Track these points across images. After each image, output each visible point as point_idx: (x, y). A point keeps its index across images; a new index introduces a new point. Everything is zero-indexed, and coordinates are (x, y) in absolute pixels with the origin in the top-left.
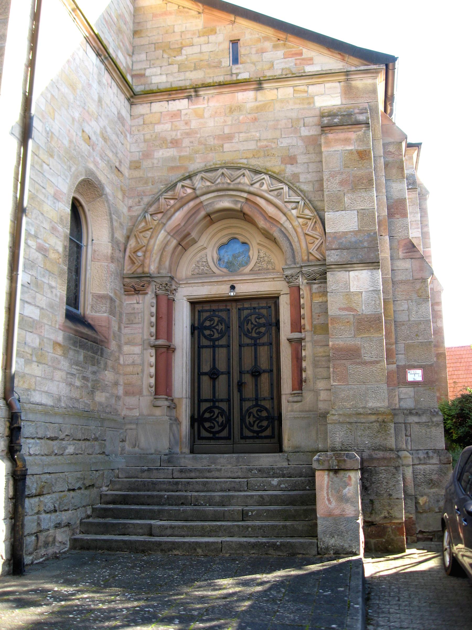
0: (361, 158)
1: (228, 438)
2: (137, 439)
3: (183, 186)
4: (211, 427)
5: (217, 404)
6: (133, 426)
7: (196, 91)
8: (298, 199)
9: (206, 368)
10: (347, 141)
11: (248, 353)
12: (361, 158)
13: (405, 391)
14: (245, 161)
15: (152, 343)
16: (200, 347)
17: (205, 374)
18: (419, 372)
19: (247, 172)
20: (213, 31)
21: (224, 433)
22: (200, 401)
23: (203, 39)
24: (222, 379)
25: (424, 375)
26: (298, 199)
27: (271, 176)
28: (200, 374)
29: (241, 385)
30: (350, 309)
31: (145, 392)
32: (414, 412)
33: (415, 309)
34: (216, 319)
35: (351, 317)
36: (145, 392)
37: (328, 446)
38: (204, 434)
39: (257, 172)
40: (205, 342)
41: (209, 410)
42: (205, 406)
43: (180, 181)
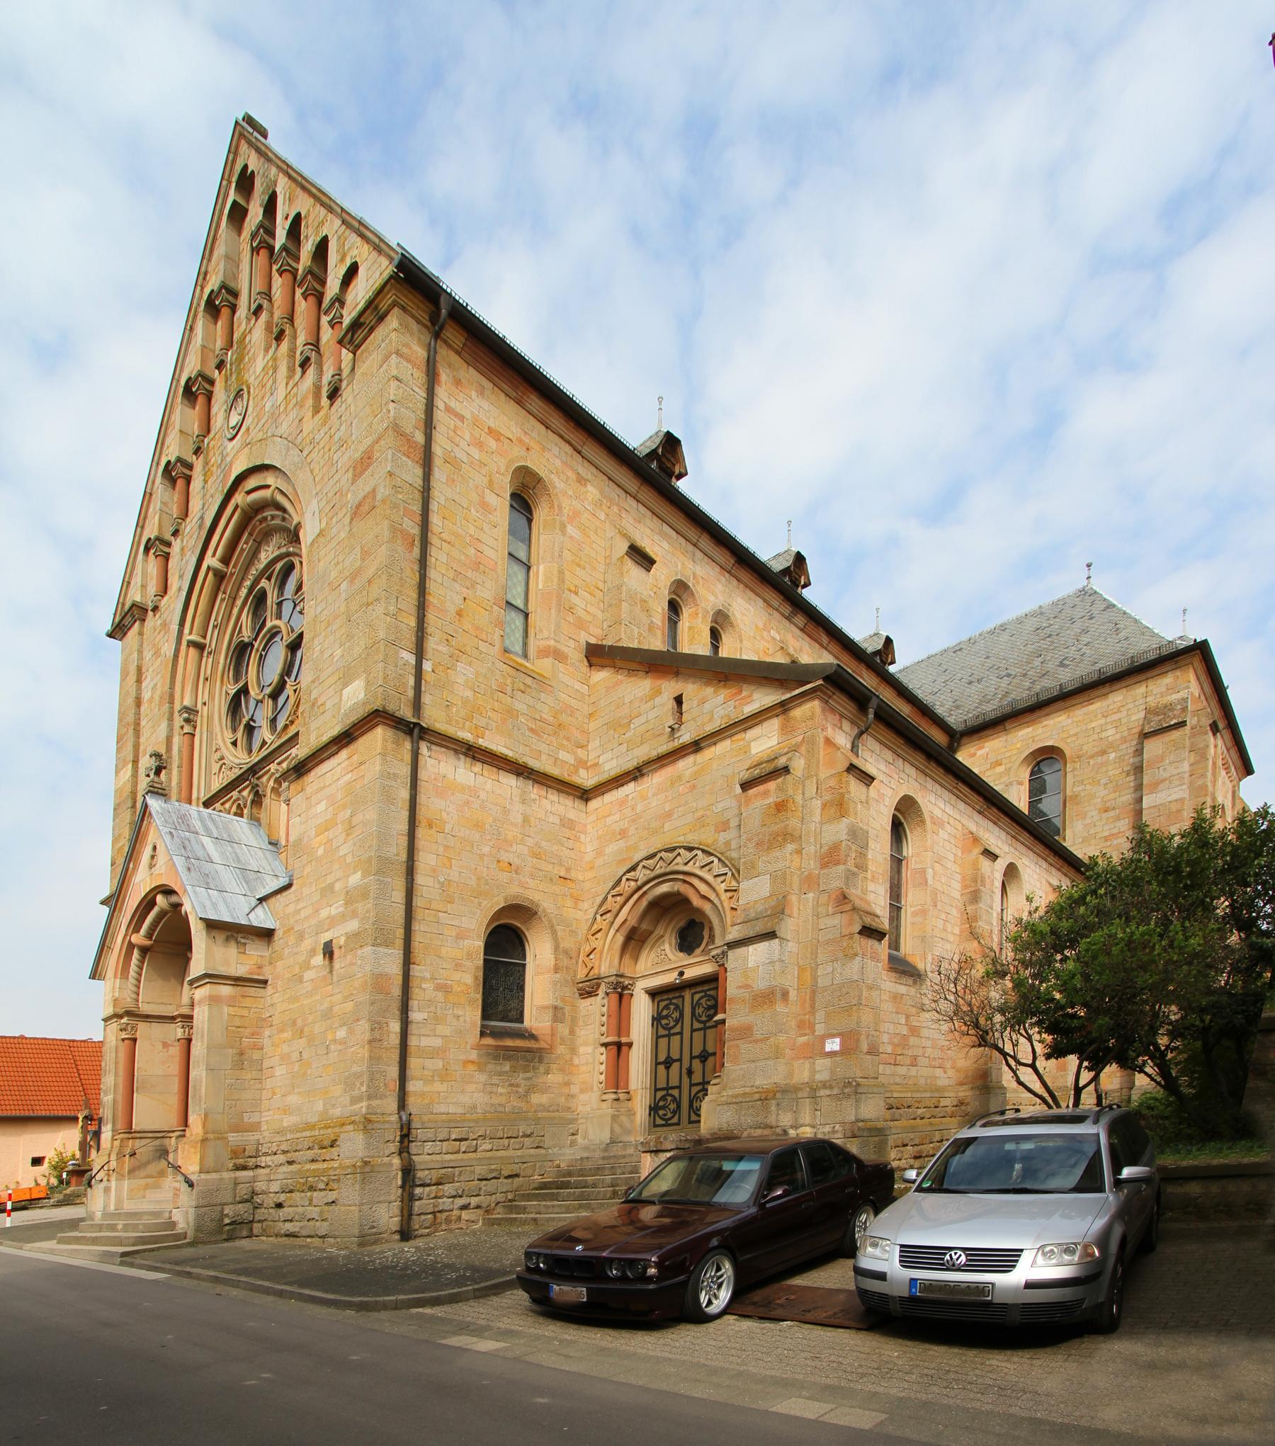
0: (779, 811)
1: (678, 1124)
2: (586, 1132)
3: (628, 880)
4: (665, 1115)
5: (670, 1092)
6: (584, 1121)
7: (640, 771)
8: (725, 870)
9: (662, 1058)
10: (766, 793)
11: (698, 1036)
12: (779, 811)
13: (822, 1064)
14: (682, 839)
15: (602, 1042)
16: (658, 1037)
17: (676, 1061)
18: (837, 1040)
19: (682, 851)
20: (658, 692)
21: (675, 1120)
22: (656, 1090)
23: (650, 704)
24: (675, 1067)
25: (842, 1044)
26: (725, 870)
27: (703, 851)
28: (657, 1064)
29: (690, 1072)
30: (747, 986)
31: (595, 1089)
32: (828, 1084)
33: (839, 971)
34: (672, 1007)
35: (747, 994)
36: (595, 1089)
37: (126, 1182)
38: (659, 1121)
39: (690, 849)
40: (662, 1032)
41: (663, 1098)
42: (660, 1094)
43: (624, 874)
